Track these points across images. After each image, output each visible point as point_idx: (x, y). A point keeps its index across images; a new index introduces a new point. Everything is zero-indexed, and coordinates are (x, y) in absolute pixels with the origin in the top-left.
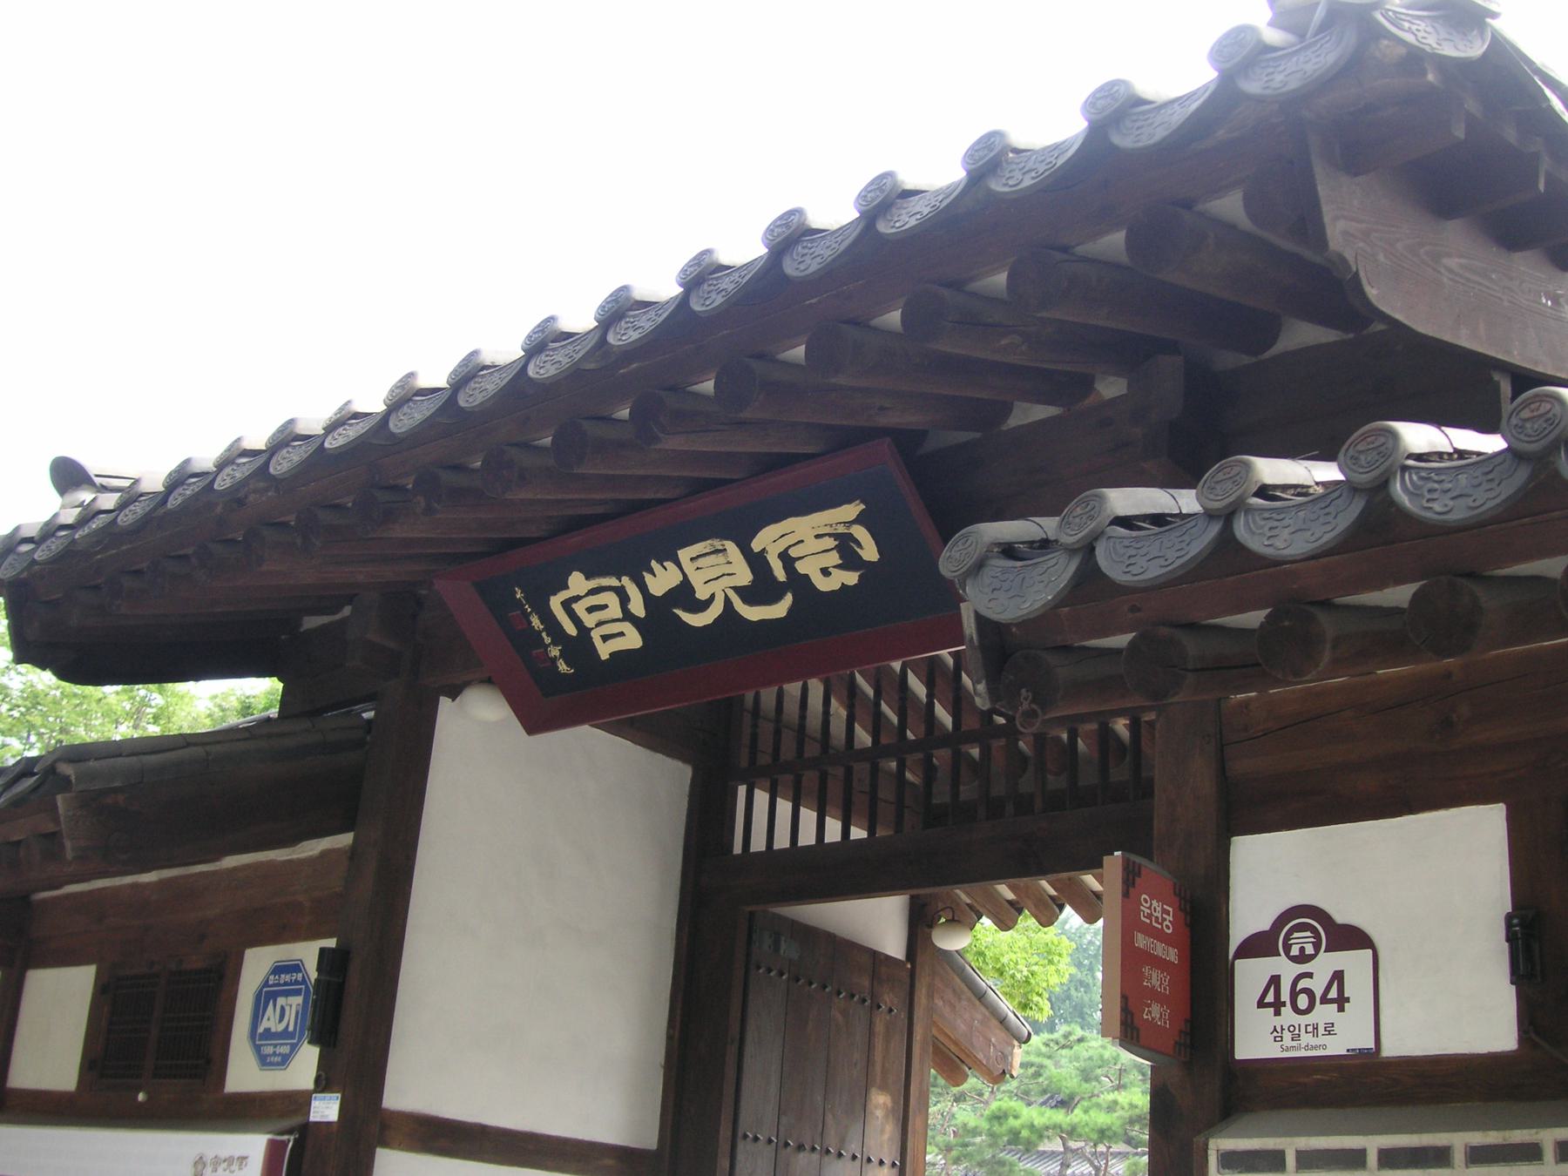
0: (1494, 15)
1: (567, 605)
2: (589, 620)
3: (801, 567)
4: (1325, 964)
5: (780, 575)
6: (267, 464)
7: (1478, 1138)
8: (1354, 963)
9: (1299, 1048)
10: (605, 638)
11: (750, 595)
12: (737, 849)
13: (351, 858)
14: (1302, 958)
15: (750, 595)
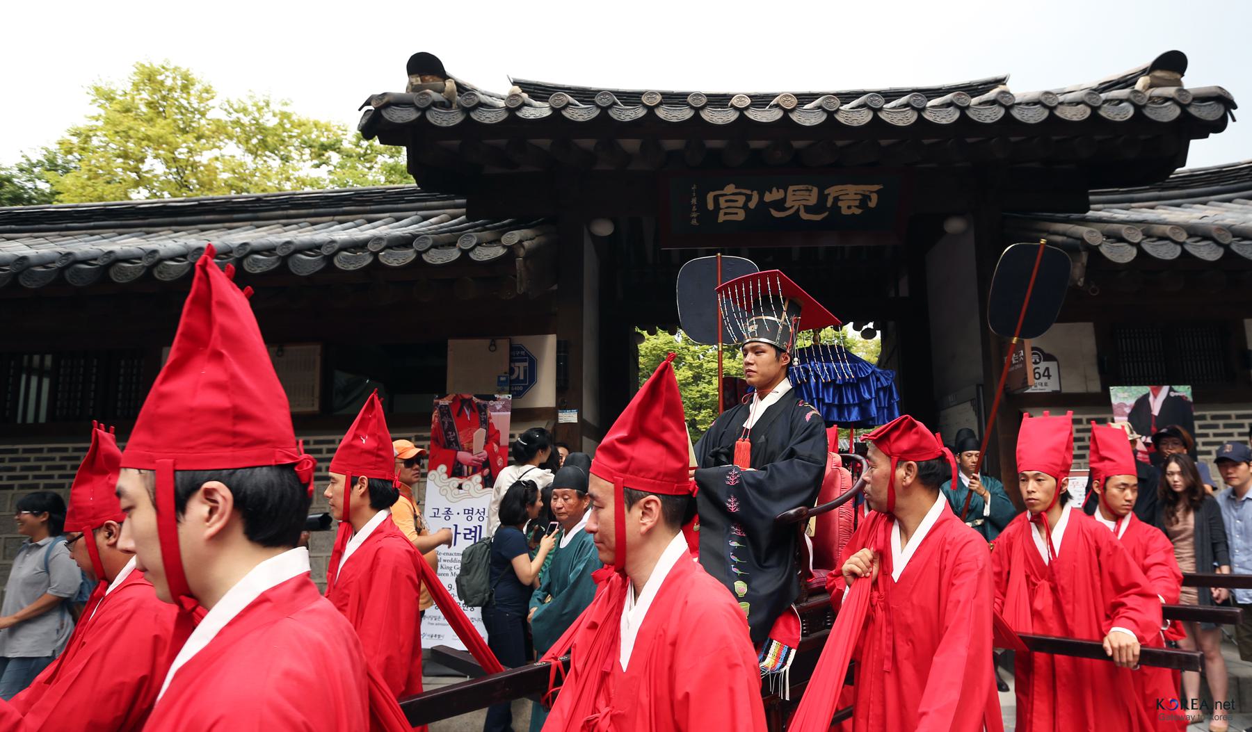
1: (716, 199)
3: (840, 204)
5: (829, 204)
8: (1052, 366)
10: (726, 214)
12: (19, 420)
15: (808, 209)
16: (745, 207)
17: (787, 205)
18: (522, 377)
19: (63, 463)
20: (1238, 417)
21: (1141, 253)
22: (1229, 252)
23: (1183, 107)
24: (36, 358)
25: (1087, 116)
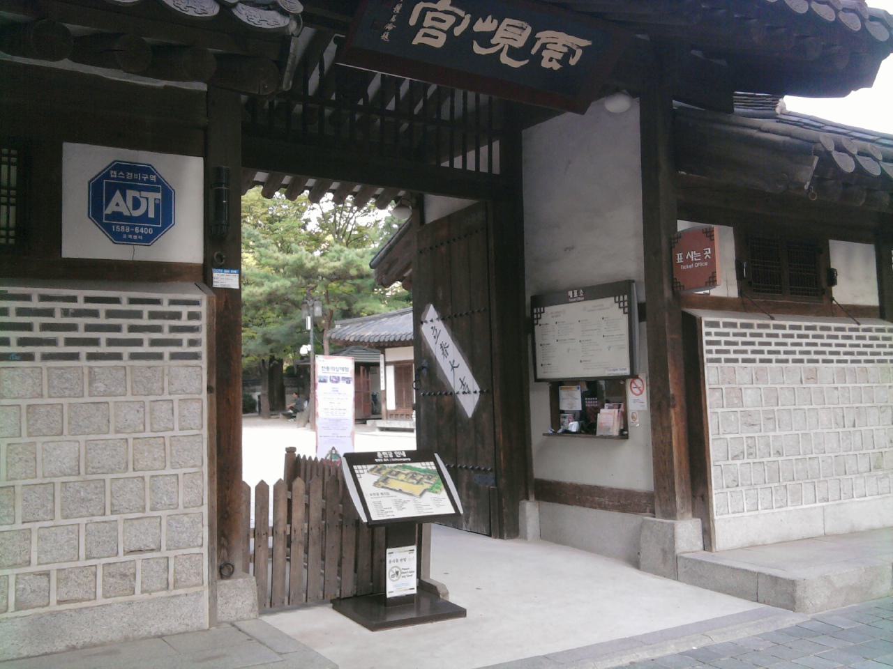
0: (484, 21)
2: (428, 22)
3: (545, 53)
5: (534, 51)
9: (125, 180)
10: (426, 35)
11: (513, 53)
15: (513, 53)
16: (449, 32)
17: (493, 41)
18: (151, 215)
24: (539, 309)
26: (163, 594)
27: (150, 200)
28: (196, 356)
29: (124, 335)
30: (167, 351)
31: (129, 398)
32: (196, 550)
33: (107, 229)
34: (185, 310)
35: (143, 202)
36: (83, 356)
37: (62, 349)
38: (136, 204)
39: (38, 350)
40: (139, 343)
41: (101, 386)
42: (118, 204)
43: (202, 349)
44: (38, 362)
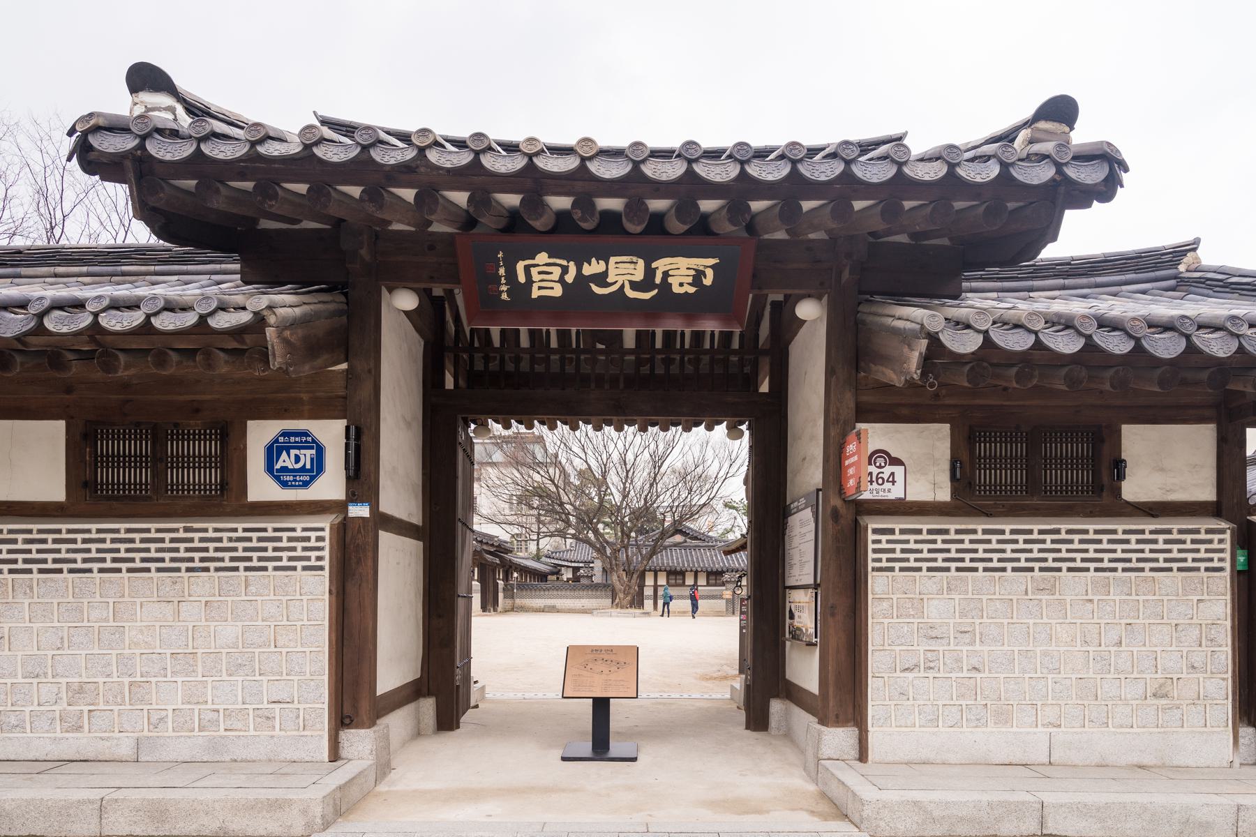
1: (527, 269)
2: (536, 277)
3: (670, 280)
4: (888, 470)
5: (658, 280)
6: (373, 145)
7: (958, 527)
8: (898, 470)
10: (540, 288)
13: (347, 379)
14: (880, 467)
15: (635, 286)
16: (561, 280)
17: (609, 280)
18: (308, 466)
19: (1209, 536)
20: (128, 531)
21: (988, 342)
22: (1090, 345)
23: (1059, 166)
25: (941, 174)
26: (295, 733)
27: (307, 455)
28: (321, 568)
29: (270, 554)
30: (299, 564)
31: (272, 597)
32: (320, 706)
33: (277, 478)
34: (313, 535)
35: (302, 457)
36: (241, 569)
37: (227, 564)
38: (297, 459)
39: (212, 565)
40: (45, 561)
41: (252, 589)
42: (285, 461)
43: (326, 563)
44: (212, 573)
